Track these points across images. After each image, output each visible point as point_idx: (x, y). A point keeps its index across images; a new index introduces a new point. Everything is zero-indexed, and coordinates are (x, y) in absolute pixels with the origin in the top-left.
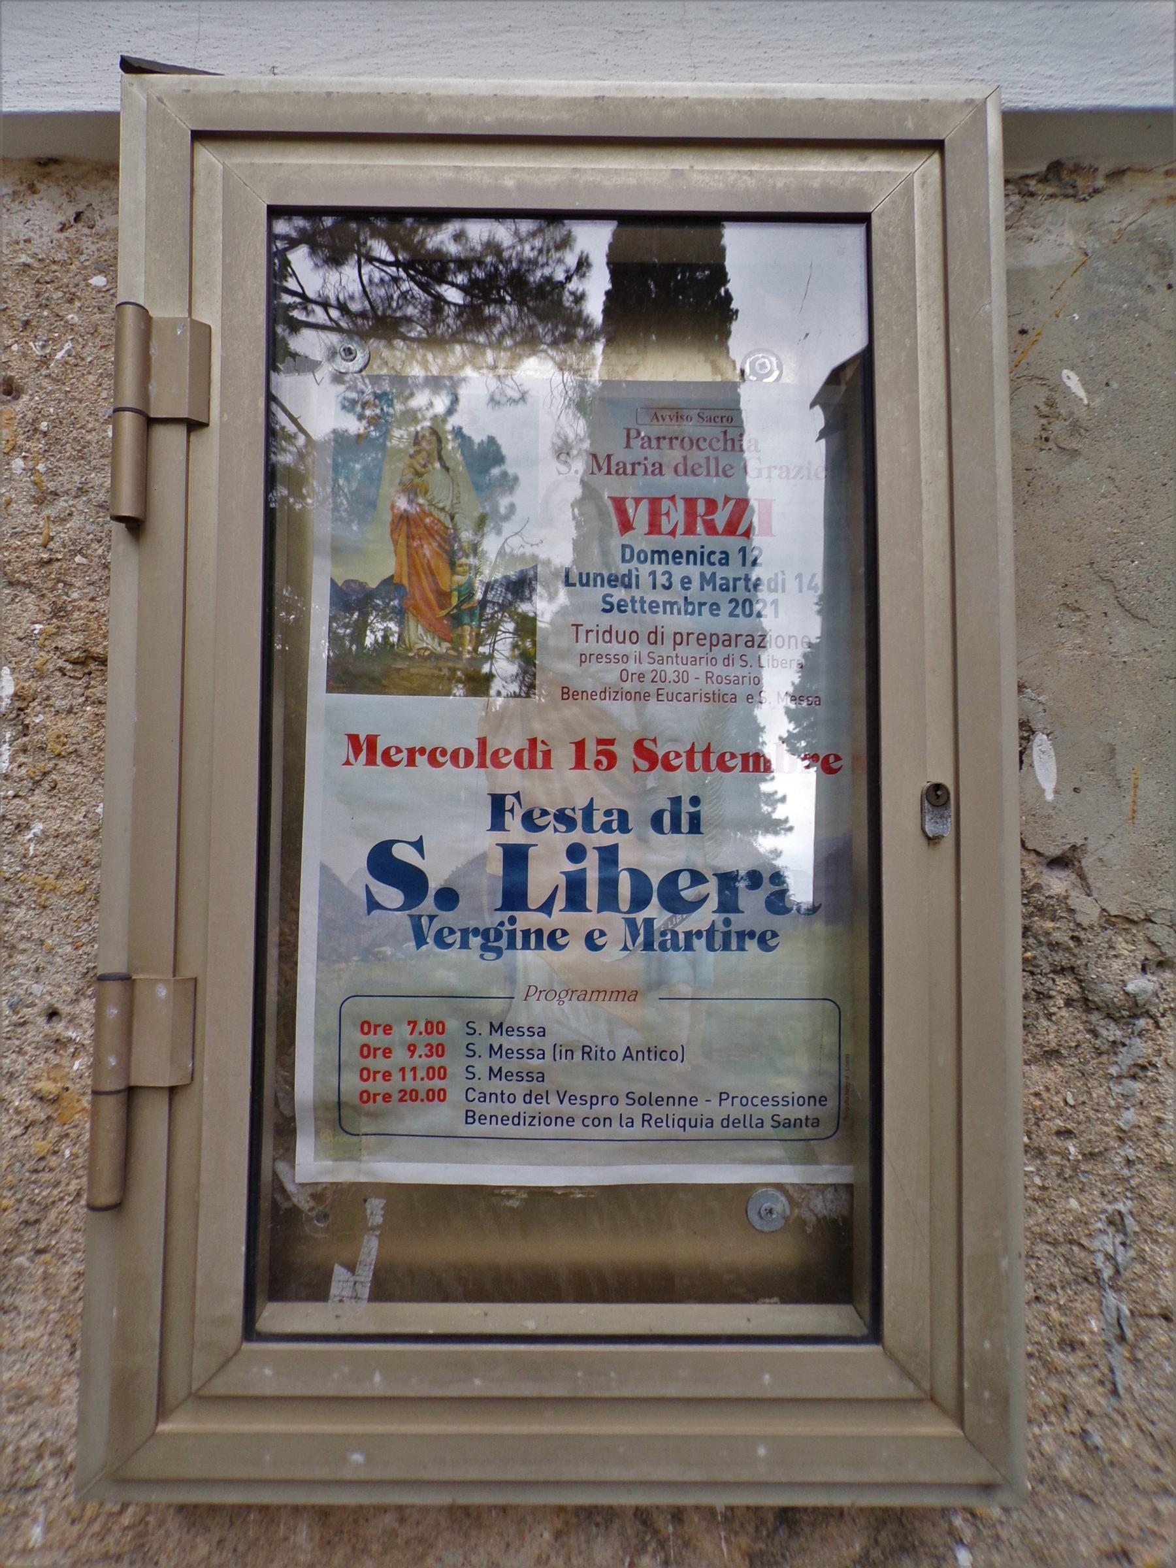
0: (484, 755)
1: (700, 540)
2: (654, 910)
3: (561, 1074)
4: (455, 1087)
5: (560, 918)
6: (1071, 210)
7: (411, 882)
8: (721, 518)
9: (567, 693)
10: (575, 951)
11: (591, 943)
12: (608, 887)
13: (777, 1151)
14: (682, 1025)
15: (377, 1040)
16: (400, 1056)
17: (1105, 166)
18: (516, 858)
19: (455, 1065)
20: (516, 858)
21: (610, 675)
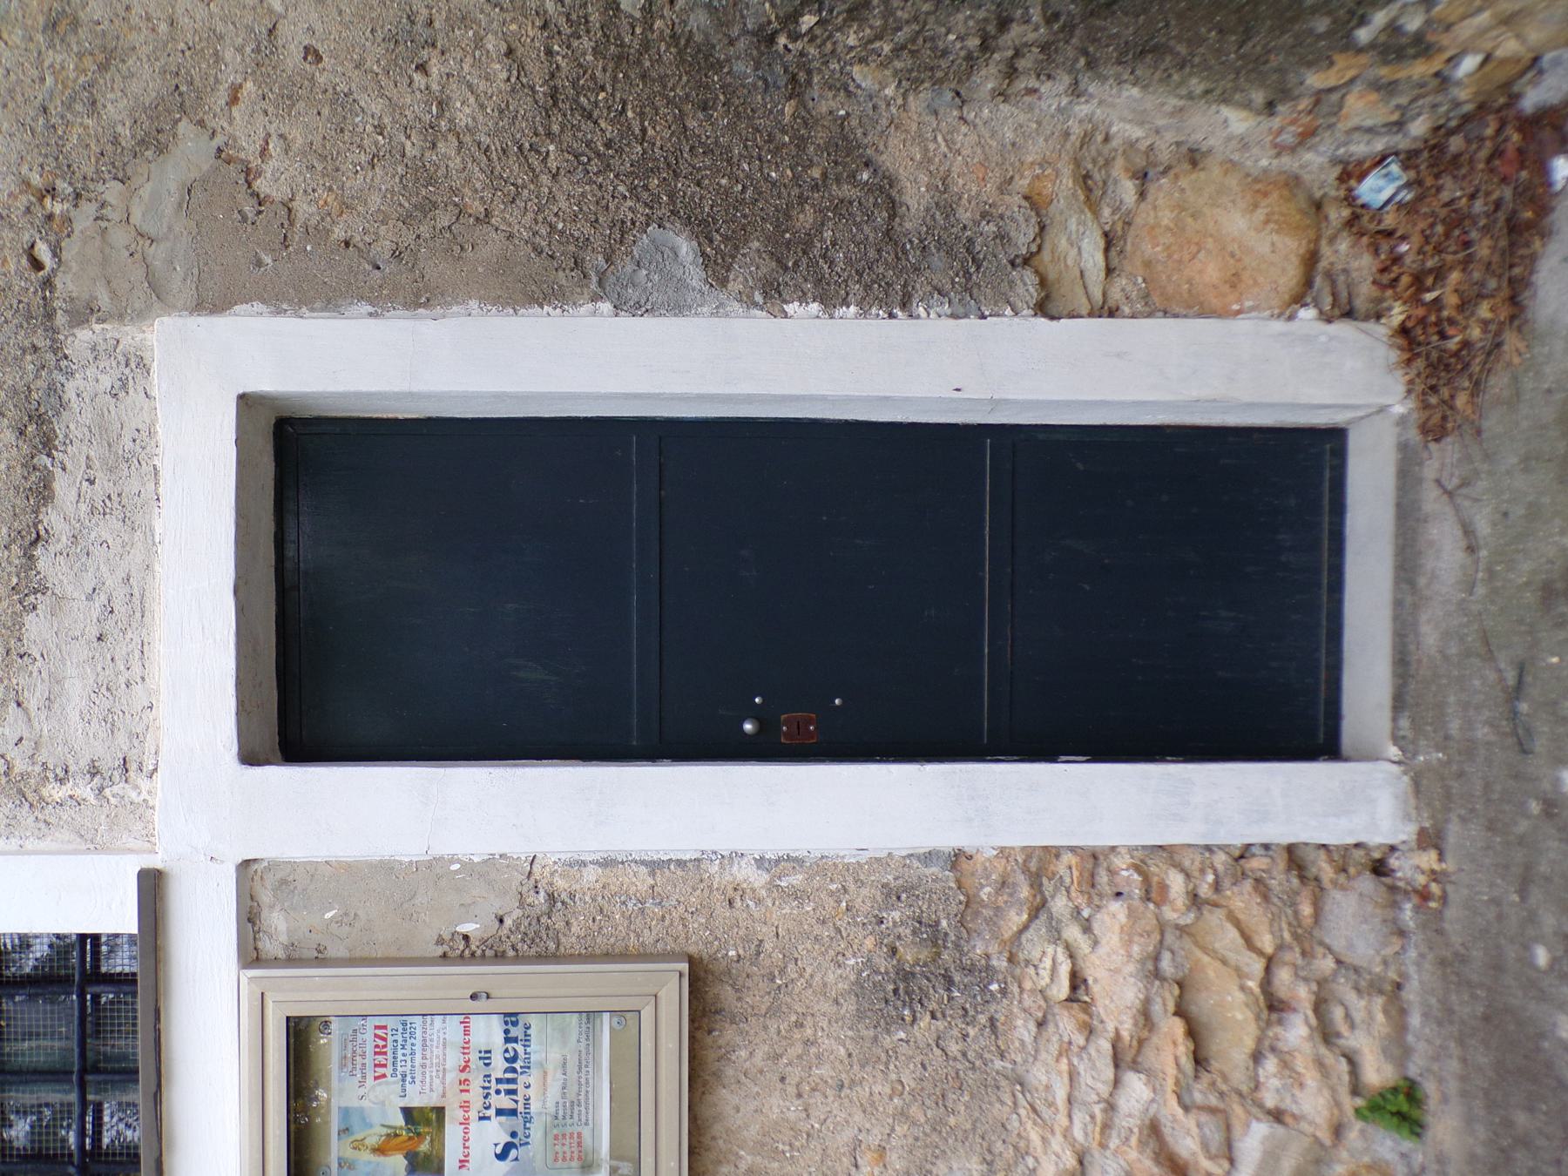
0: (465, 1122)
1: (389, 1050)
2: (517, 1066)
3: (571, 1095)
4: (576, 1129)
5: (520, 1097)
6: (265, 914)
7: (508, 1147)
8: (381, 1043)
9: (444, 1095)
10: (530, 1092)
11: (528, 1087)
12: (509, 1081)
13: (598, 1022)
14: (555, 1055)
15: (560, 1156)
16: (566, 1148)
17: (249, 903)
18: (500, 1112)
19: (569, 1130)
20: (500, 1112)
21: (437, 1082)
